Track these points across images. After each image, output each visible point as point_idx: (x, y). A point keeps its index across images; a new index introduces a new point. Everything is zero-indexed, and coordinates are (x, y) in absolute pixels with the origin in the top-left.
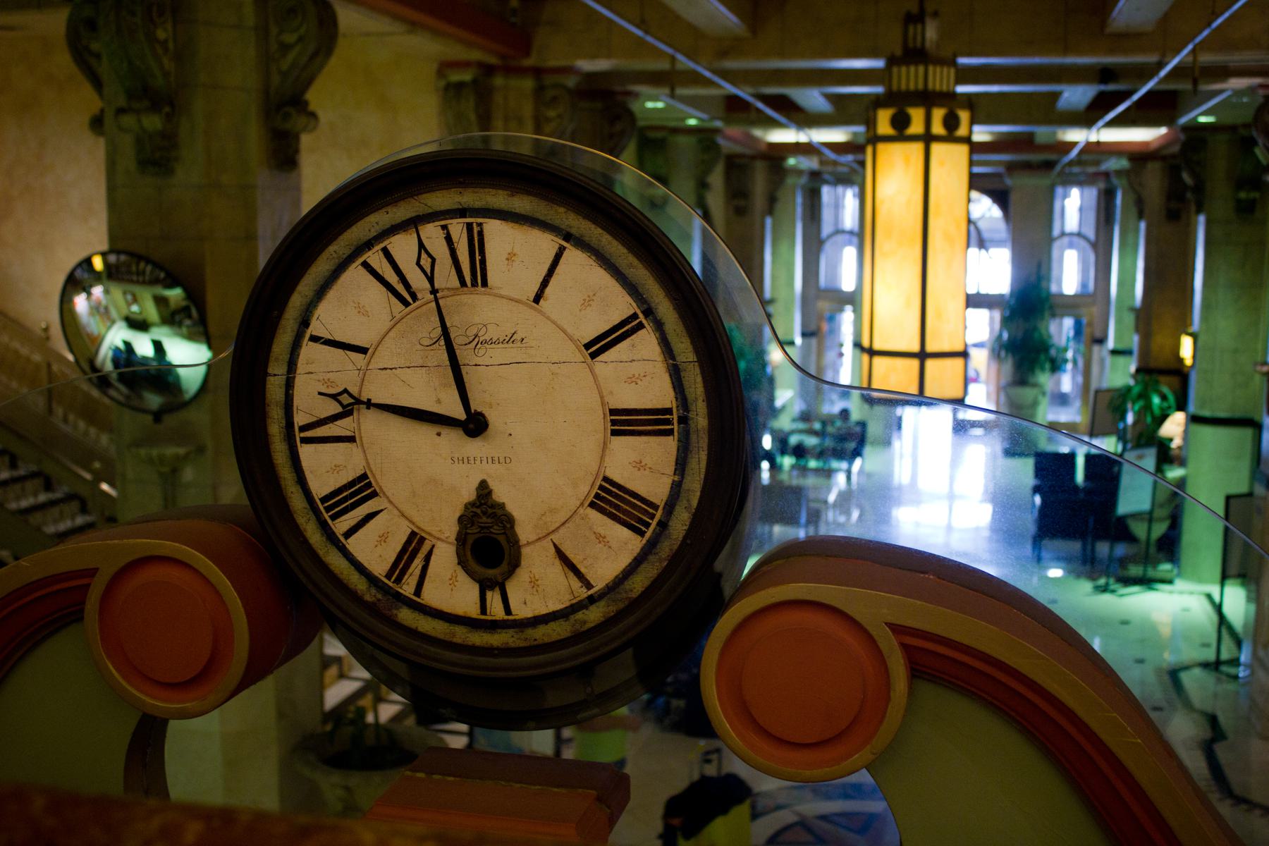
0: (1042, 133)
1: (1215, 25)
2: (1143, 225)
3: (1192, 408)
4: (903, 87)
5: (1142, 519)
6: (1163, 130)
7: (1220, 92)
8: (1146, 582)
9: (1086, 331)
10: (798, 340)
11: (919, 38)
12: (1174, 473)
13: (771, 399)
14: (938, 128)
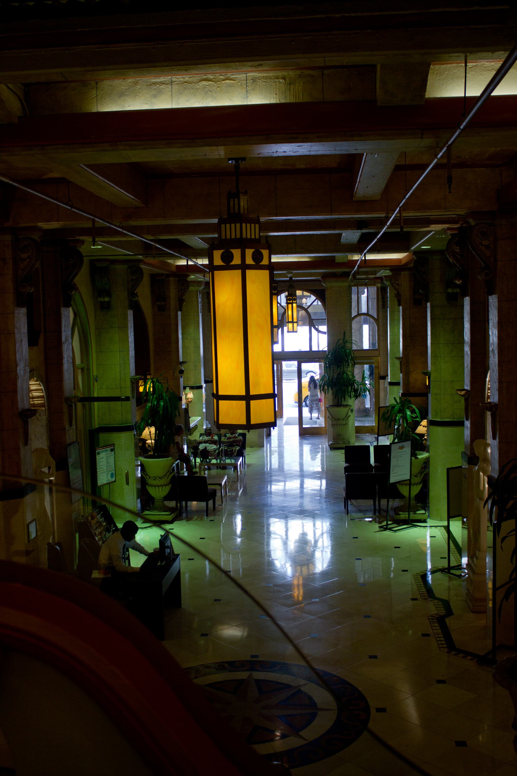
0: (339, 257)
1: (407, 197)
2: (401, 308)
3: (430, 417)
4: (228, 237)
5: (406, 485)
6: (405, 254)
7: (430, 232)
8: (411, 523)
9: (376, 371)
10: (204, 385)
11: (237, 207)
12: (423, 456)
13: (187, 423)
14: (249, 261)
